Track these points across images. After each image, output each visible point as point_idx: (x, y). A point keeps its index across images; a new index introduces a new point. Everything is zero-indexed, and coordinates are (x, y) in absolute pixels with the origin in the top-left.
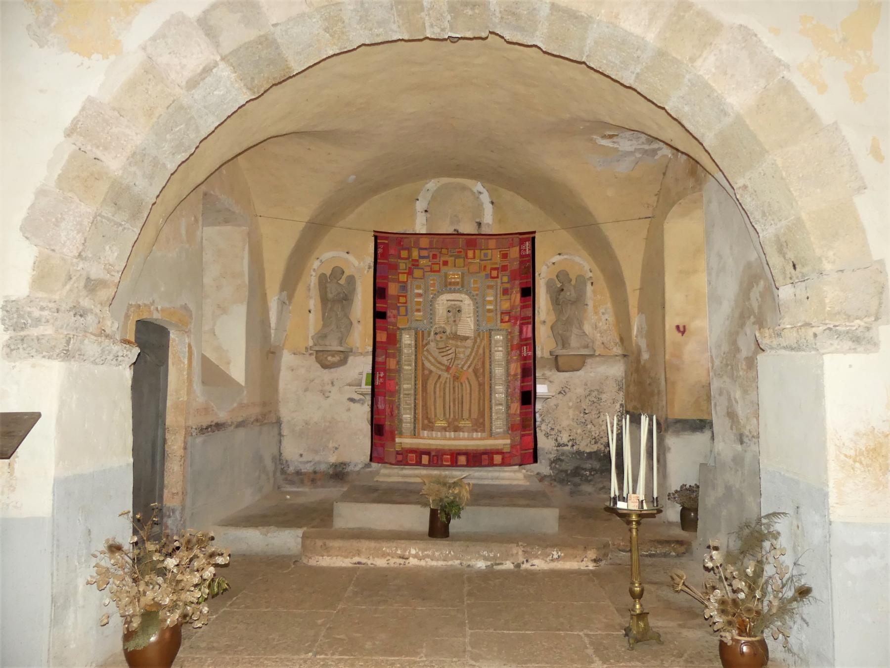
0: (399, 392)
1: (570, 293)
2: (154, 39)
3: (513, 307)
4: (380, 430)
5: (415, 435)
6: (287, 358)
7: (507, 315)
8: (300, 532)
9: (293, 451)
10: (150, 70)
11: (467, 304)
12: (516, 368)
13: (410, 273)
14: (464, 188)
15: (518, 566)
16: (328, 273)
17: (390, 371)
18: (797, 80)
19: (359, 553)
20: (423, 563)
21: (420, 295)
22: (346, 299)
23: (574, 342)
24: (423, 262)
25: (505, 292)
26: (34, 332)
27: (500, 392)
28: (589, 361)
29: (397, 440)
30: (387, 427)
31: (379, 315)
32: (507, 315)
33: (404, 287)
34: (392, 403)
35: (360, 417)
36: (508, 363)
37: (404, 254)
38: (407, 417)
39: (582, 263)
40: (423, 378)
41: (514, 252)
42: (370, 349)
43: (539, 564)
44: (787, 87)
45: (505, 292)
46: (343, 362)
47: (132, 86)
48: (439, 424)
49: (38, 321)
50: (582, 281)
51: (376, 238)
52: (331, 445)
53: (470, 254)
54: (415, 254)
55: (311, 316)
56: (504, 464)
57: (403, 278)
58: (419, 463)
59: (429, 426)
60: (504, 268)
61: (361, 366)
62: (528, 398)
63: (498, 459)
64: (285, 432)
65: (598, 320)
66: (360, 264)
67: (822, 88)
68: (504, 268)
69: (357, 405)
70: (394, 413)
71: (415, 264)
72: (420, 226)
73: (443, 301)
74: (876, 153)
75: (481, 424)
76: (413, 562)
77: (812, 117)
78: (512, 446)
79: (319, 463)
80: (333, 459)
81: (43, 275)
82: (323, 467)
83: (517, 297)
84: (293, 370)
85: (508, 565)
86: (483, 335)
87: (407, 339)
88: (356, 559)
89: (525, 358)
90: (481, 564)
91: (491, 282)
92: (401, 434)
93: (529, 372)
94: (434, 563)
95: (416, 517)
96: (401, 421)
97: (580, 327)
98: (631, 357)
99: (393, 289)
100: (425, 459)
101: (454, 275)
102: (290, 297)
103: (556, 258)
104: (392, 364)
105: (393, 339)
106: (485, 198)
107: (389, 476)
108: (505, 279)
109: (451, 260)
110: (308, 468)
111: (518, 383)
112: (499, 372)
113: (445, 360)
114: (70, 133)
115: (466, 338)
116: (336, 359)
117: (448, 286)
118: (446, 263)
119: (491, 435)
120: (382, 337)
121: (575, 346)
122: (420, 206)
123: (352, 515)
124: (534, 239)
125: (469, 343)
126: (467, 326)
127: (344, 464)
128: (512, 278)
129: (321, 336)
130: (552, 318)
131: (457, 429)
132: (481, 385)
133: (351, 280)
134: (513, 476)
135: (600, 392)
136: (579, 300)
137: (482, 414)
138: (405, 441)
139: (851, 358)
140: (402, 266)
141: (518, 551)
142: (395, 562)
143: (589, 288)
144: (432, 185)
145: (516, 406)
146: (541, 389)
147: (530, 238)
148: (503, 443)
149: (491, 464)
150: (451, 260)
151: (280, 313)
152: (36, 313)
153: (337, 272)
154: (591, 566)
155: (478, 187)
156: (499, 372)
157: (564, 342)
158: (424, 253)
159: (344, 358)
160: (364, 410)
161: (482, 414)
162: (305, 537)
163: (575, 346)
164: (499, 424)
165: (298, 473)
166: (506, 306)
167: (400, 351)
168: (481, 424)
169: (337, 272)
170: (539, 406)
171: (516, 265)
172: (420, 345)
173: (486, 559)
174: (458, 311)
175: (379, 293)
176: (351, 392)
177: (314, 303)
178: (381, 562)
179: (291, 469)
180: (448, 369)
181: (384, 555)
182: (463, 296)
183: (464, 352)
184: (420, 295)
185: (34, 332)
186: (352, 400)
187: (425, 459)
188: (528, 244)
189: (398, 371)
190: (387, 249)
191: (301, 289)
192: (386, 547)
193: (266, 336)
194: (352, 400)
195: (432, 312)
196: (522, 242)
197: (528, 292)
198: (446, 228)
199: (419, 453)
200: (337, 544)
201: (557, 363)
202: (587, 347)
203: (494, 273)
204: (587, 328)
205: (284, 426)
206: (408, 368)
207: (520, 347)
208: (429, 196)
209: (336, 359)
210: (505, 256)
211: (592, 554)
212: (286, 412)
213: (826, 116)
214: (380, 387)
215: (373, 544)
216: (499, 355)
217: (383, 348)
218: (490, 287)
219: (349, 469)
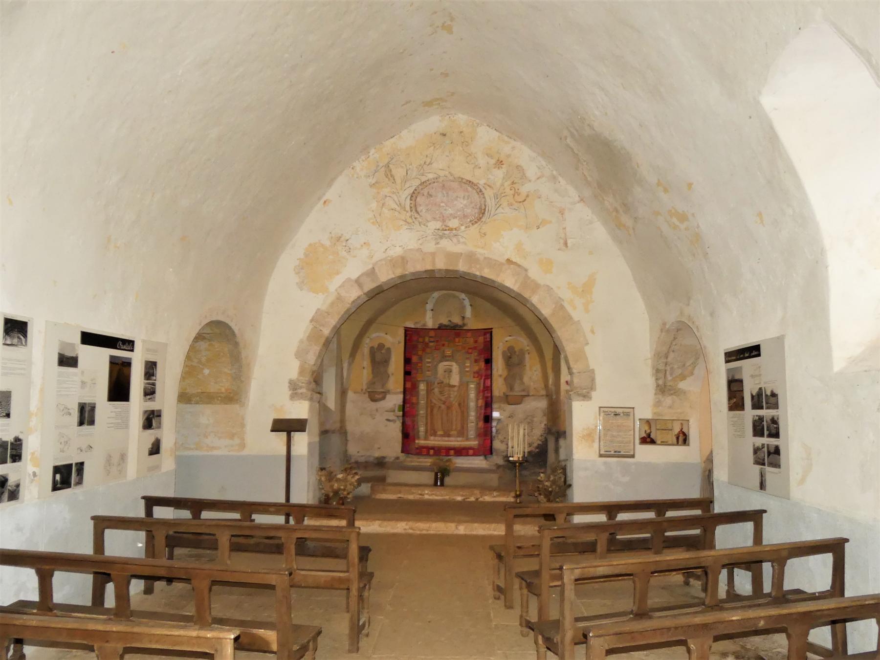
0: (418, 415)
1: (515, 360)
2: (340, 287)
3: (480, 370)
4: (407, 435)
5: (426, 439)
6: (350, 395)
7: (478, 374)
8: (369, 485)
9: (355, 450)
10: (339, 298)
11: (455, 367)
12: (481, 402)
13: (424, 350)
14: (455, 297)
15: (477, 499)
16: (376, 346)
17: (413, 404)
18: (566, 305)
19: (400, 492)
20: (431, 498)
21: (429, 363)
22: (386, 362)
23: (517, 387)
24: (431, 344)
25: (476, 361)
26: (300, 391)
27: (472, 416)
28: (527, 398)
29: (417, 441)
30: (411, 434)
31: (407, 373)
32: (478, 374)
33: (421, 358)
34: (413, 421)
35: (395, 431)
36: (477, 400)
37: (421, 340)
38: (422, 429)
39: (522, 342)
40: (430, 407)
41: (481, 339)
42: (402, 390)
43: (487, 499)
44: (562, 307)
45: (476, 361)
46: (384, 398)
47: (332, 304)
48: (440, 433)
49: (301, 387)
50: (522, 352)
51: (406, 331)
52: (376, 446)
53: (457, 340)
54: (427, 339)
55: (365, 371)
56: (475, 455)
57: (420, 353)
58: (428, 454)
59: (434, 434)
60: (475, 348)
61: (395, 400)
62: (488, 419)
63: (471, 452)
64: (349, 438)
65: (532, 375)
66: (395, 342)
67: (575, 308)
68: (475, 348)
69: (391, 423)
70: (414, 426)
71: (427, 345)
72: (430, 324)
73: (442, 366)
74: (593, 332)
75: (462, 433)
76: (426, 497)
77: (571, 318)
78: (479, 444)
79: (369, 456)
80: (377, 454)
81: (302, 372)
82: (371, 459)
83: (482, 364)
84: (355, 402)
85: (472, 499)
86: (464, 385)
87: (422, 387)
88: (399, 495)
89: (487, 397)
90: (459, 498)
91: (468, 356)
92: (419, 438)
93: (488, 405)
94: (436, 498)
95: (428, 477)
96: (419, 432)
97: (521, 379)
98: (548, 396)
99: (415, 359)
100: (432, 452)
101: (448, 352)
102: (353, 361)
103: (508, 338)
104: (414, 400)
105: (415, 387)
106: (467, 303)
107: (412, 462)
108: (476, 354)
109: (446, 343)
110: (362, 460)
111: (483, 411)
112: (472, 404)
113: (443, 398)
114: (311, 321)
115: (454, 386)
116: (381, 396)
117: (444, 358)
118: (443, 345)
119: (468, 439)
120: (409, 385)
121: (517, 391)
122: (429, 306)
123: (394, 476)
124: (491, 333)
125: (456, 389)
126: (455, 380)
127: (384, 458)
128: (480, 353)
129: (371, 383)
130: (505, 373)
131: (449, 436)
132: (463, 412)
133: (389, 350)
134: (479, 462)
135: (533, 416)
136: (521, 363)
137: (463, 427)
138: (421, 442)
139: (582, 403)
140: (420, 346)
141: (477, 492)
142: (418, 497)
143: (527, 356)
144: (436, 295)
145: (481, 424)
146: (496, 414)
147: (489, 332)
148: (474, 443)
149: (467, 455)
150: (446, 343)
151: (348, 369)
152: (301, 384)
153: (381, 346)
154: (512, 500)
155: (463, 296)
156: (472, 404)
157: (511, 388)
158: (432, 340)
159: (383, 395)
160: (398, 425)
161: (463, 427)
162: (372, 487)
163: (517, 391)
164: (472, 433)
165: (357, 462)
166: (476, 368)
167: (418, 393)
168: (462, 433)
169: (381, 346)
170: (494, 424)
171: (481, 346)
172: (429, 391)
173: (462, 496)
174: (452, 372)
175: (407, 361)
176: (391, 416)
177: (367, 363)
178: (411, 497)
179: (353, 460)
180: (444, 403)
181: (413, 493)
182: (454, 364)
183: (454, 394)
184: (429, 363)
185: (300, 391)
186: (388, 420)
187: (432, 452)
188: (488, 336)
189: (418, 403)
190: (412, 337)
191: (358, 356)
192: (413, 490)
193: (342, 384)
194: (388, 420)
195: (436, 373)
196: (485, 334)
197: (489, 361)
198: (444, 321)
199: (428, 448)
200: (390, 488)
201: (508, 399)
202: (523, 390)
203: (470, 351)
204: (526, 379)
205: (348, 435)
206: (422, 402)
207: (483, 391)
208: (434, 300)
209: (381, 396)
210: (476, 342)
211: (513, 494)
212: (350, 427)
213: (576, 318)
214: (407, 410)
215: (407, 488)
216: (472, 395)
217: (409, 391)
218: (467, 359)
219: (387, 460)
